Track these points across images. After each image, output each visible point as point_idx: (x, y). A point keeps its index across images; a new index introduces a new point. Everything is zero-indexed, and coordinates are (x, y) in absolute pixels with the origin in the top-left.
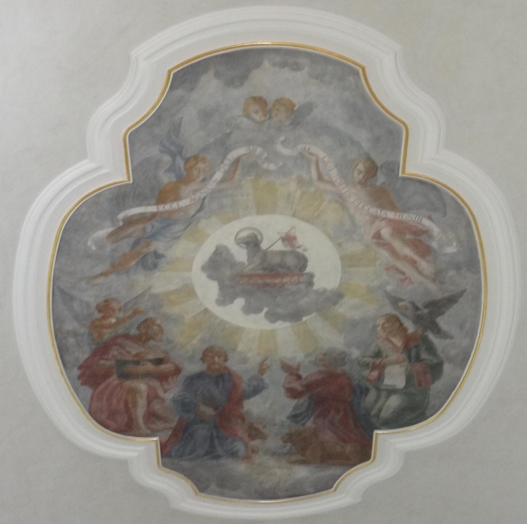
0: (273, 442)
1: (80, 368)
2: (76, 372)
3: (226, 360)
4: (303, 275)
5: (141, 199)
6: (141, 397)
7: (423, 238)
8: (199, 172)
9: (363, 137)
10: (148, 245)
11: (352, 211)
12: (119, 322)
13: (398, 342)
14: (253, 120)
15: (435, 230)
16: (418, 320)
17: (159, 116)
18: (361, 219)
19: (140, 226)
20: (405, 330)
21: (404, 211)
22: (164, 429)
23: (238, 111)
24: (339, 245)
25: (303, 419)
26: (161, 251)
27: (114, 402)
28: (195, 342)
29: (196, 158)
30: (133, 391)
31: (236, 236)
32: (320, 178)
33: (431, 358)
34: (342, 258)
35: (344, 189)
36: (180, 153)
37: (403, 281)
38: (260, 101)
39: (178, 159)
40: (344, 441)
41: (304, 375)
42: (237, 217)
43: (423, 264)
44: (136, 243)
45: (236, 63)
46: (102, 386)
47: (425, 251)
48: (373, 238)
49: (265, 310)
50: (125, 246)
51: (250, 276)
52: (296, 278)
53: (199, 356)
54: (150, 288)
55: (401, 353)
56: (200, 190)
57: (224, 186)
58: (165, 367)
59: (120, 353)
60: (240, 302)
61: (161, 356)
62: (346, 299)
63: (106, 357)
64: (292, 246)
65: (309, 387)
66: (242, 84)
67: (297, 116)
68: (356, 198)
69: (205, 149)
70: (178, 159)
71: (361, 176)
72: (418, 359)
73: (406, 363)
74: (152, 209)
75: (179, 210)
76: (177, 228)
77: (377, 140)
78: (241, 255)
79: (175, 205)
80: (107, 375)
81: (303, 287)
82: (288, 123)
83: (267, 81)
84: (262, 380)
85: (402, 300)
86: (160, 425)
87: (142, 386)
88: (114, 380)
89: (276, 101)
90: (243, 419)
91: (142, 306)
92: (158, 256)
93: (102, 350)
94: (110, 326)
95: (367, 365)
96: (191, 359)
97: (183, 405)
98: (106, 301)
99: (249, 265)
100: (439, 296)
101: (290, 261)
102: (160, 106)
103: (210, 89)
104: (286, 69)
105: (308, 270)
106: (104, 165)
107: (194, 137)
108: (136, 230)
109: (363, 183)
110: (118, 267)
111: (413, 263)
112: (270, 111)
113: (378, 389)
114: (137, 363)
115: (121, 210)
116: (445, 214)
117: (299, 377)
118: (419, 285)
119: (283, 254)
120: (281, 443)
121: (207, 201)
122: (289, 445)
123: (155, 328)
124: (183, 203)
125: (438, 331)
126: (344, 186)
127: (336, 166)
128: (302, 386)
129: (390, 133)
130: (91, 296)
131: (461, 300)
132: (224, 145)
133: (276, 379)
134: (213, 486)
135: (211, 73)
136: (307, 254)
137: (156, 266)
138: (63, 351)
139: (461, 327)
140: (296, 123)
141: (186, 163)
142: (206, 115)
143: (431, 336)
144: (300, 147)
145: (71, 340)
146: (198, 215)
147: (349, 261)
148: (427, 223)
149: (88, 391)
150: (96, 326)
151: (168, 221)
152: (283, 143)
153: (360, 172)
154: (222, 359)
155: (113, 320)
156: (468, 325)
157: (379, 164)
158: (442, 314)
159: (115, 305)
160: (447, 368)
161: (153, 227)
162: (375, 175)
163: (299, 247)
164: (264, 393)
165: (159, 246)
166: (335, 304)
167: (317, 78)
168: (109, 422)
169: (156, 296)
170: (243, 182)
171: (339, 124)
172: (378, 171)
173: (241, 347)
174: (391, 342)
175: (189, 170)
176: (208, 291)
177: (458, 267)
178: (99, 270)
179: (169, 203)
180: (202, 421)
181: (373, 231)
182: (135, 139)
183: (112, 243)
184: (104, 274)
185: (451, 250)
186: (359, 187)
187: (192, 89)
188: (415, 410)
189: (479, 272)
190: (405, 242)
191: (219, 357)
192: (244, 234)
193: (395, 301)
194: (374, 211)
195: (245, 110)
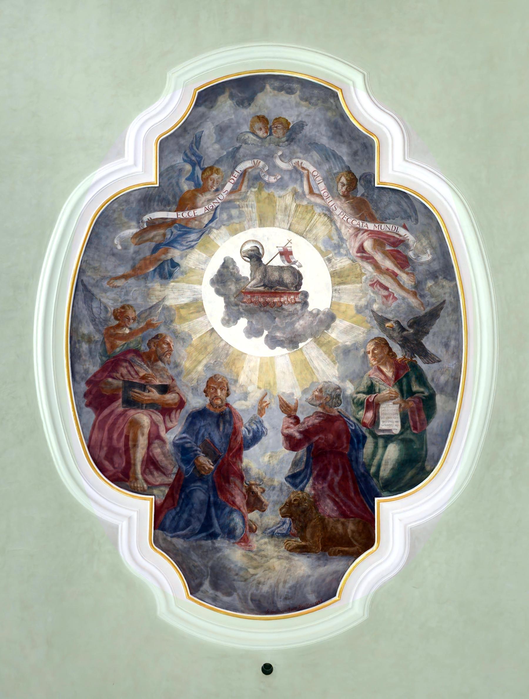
0: (271, 517)
1: (88, 383)
2: (83, 387)
3: (228, 395)
4: (298, 293)
5: (165, 205)
6: (143, 435)
7: (401, 248)
8: (213, 182)
9: (343, 151)
10: (166, 252)
11: (338, 224)
12: (133, 333)
13: (389, 372)
14: (257, 136)
15: (410, 238)
16: (405, 343)
17: (185, 128)
18: (346, 232)
19: (161, 231)
20: (394, 355)
21: (383, 221)
22: (161, 485)
23: (246, 128)
24: (329, 260)
25: (301, 482)
26: (177, 260)
27: (115, 436)
28: (200, 368)
29: (211, 168)
30: (135, 424)
31: (242, 247)
32: (311, 192)
33: (422, 389)
34: (333, 275)
35: (331, 203)
36: (199, 163)
37: (386, 297)
38: (263, 119)
39: (197, 168)
40: (346, 516)
41: (302, 418)
42: (243, 229)
43: (404, 277)
44: (155, 249)
45: (245, 87)
46: (106, 411)
47: (403, 262)
48: (358, 252)
49: (266, 333)
50: (146, 249)
51: (252, 293)
52: (292, 297)
53: (203, 386)
54: (164, 299)
55: (393, 386)
56: (214, 199)
57: (233, 197)
58: (170, 398)
59: (129, 371)
60: (243, 322)
61: (168, 382)
62: (337, 321)
63: (115, 374)
64: (289, 261)
65: (307, 434)
66: (250, 104)
67: (292, 133)
68: (340, 209)
69: (219, 161)
70: (197, 168)
71: (344, 189)
72: (411, 393)
73: (398, 400)
74: (173, 215)
75: (195, 218)
76: (193, 236)
77: (355, 154)
78: (244, 269)
79: (191, 214)
80: (112, 399)
81: (298, 307)
82: (284, 139)
83: (268, 102)
84: (261, 422)
85: (389, 320)
86: (158, 478)
87: (144, 419)
88: (118, 406)
89: (276, 119)
90: (242, 478)
91: (155, 319)
92: (174, 265)
93: (111, 365)
94: (124, 337)
95: (362, 404)
96: (194, 389)
97: (183, 451)
98: (123, 307)
99: (252, 280)
100: (422, 312)
101: (287, 278)
102: (187, 119)
103: (225, 107)
104: (283, 92)
105: (303, 288)
106: (137, 167)
107: (212, 149)
108: (157, 234)
109: (346, 196)
110: (137, 272)
111: (394, 276)
112: (271, 129)
113: (375, 437)
114: (143, 388)
115: (146, 213)
116: (417, 220)
117: (297, 421)
118: (403, 303)
119: (281, 269)
120: (280, 518)
121: (218, 211)
122: (288, 520)
123: (165, 346)
124: (199, 212)
125: (425, 354)
126: (331, 199)
127: (324, 180)
128: (300, 432)
129: (364, 147)
130: (110, 300)
131: (442, 313)
132: (234, 158)
133: (275, 423)
134: (206, 585)
135: (227, 94)
136: (301, 270)
137: (171, 275)
138: (74, 356)
139: (446, 345)
140: (291, 140)
141: (203, 174)
142: (221, 130)
143: (420, 362)
144: (294, 161)
145: (85, 347)
146: (210, 225)
147: (339, 278)
148: (402, 232)
149: (91, 415)
150: (111, 335)
151: (184, 229)
152: (280, 157)
153: (343, 185)
154: (224, 392)
155: (127, 331)
156: (453, 343)
157: (358, 177)
158: (427, 333)
159: (131, 314)
160: (439, 399)
161: (172, 232)
162: (355, 188)
163: (295, 263)
164: (264, 440)
165: (175, 253)
166: (328, 327)
167: (306, 100)
168: (107, 464)
169: (167, 309)
170: (249, 193)
171: (324, 141)
172: (358, 183)
173: (242, 379)
174: (381, 371)
175: (205, 180)
176: (215, 305)
177: (434, 276)
178: (121, 271)
179: (188, 210)
180: (201, 478)
181: (357, 245)
182: (165, 145)
183: (136, 245)
184: (125, 277)
185: (426, 258)
186: (343, 199)
187: (212, 107)
188: (413, 470)
189: (454, 279)
190: (386, 254)
191: (222, 389)
192: (248, 247)
193: (382, 321)
194: (356, 223)
195: (252, 127)
